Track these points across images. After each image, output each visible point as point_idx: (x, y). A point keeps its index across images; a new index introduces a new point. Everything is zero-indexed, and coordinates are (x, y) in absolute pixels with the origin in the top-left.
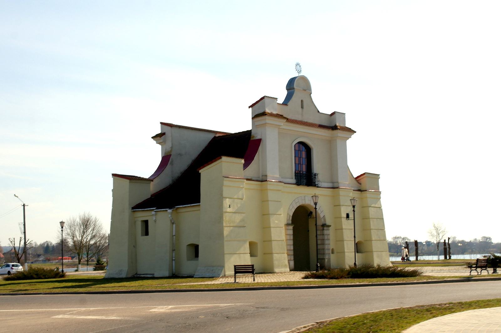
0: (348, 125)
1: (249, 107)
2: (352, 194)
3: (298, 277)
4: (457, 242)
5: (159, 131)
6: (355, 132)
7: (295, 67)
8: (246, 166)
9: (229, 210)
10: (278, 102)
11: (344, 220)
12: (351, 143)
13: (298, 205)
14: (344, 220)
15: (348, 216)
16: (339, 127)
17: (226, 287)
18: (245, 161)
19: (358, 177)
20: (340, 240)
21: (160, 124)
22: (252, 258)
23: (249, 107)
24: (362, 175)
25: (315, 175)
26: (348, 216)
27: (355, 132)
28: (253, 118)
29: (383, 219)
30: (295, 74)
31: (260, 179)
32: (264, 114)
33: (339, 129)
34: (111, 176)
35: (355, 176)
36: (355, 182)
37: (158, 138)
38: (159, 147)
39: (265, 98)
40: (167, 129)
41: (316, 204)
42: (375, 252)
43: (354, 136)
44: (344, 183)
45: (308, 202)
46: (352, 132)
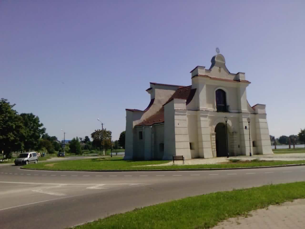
0: (246, 79)
1: (190, 72)
2: (250, 116)
3: (223, 160)
4: (107, 131)
5: (149, 87)
6: (250, 83)
7: (216, 50)
8: (187, 103)
9: (178, 126)
10: (206, 68)
11: (244, 129)
12: (249, 89)
13: (218, 123)
14: (244, 129)
15: (246, 127)
16: (241, 81)
17: (235, 167)
18: (187, 100)
19: (254, 106)
20: (242, 140)
21: (150, 84)
22: (192, 150)
23: (190, 72)
24: (255, 105)
25: (228, 106)
26: (246, 127)
27: (250, 83)
28: (192, 78)
29: (268, 128)
30: (215, 54)
31: (196, 109)
32: (197, 75)
33: (241, 82)
34: (125, 110)
35: (252, 106)
36: (252, 109)
37: (149, 90)
38: (150, 95)
39: (198, 67)
40: (153, 86)
41: (226, 122)
42: (177, 142)
43: (250, 85)
44: (244, 109)
45: (223, 121)
46: (248, 82)
